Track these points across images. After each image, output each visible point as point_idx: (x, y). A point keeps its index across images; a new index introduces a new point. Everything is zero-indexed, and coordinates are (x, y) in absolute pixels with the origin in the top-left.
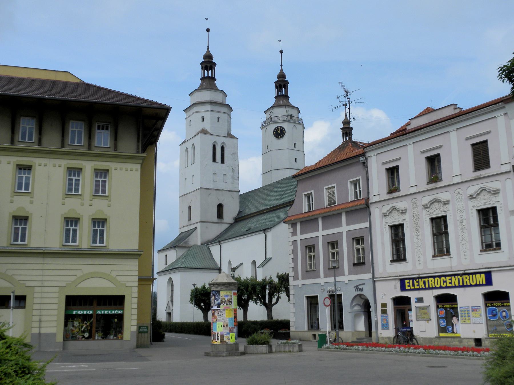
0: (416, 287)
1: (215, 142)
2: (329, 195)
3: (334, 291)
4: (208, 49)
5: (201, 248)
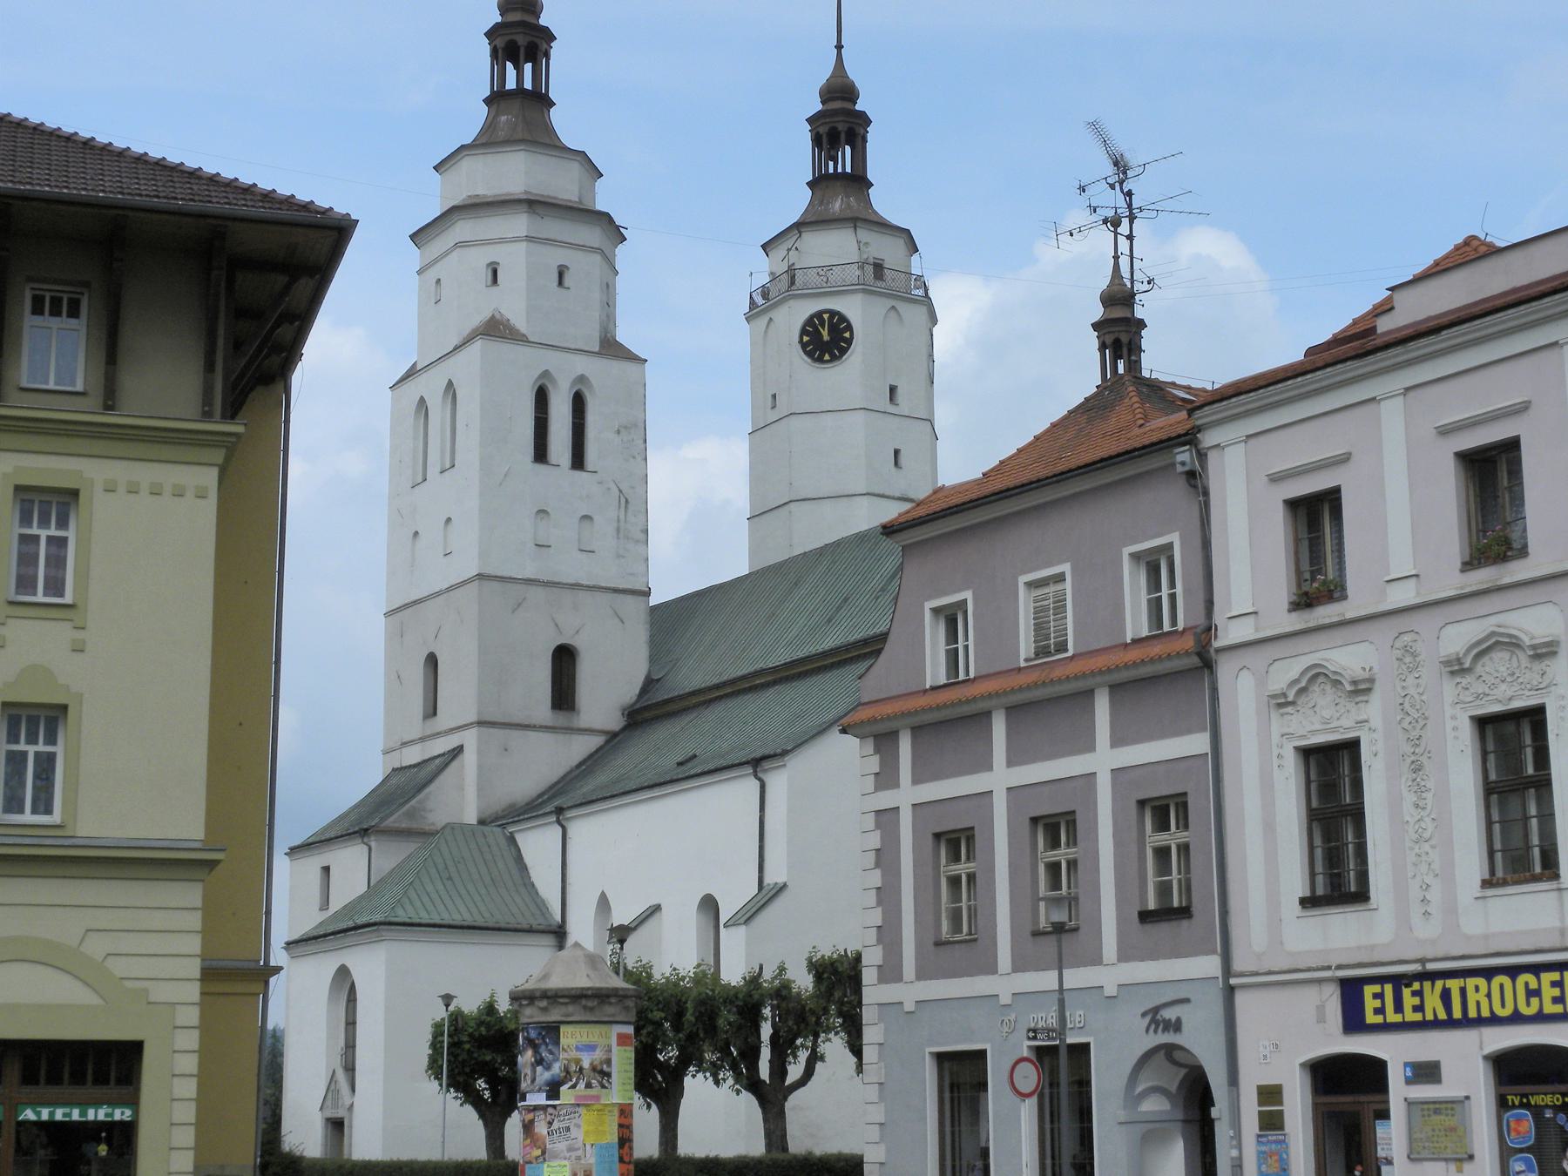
0: (1411, 1016)
1: (546, 374)
2: (1040, 612)
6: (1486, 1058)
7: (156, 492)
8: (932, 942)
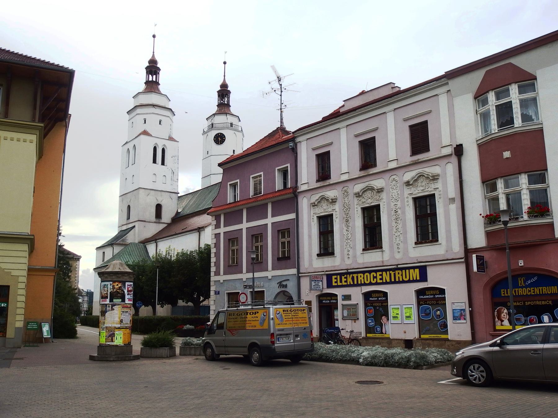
0: (344, 283)
1: (156, 144)
2: (255, 185)
3: (251, 286)
4: (153, 55)
5: (138, 247)
6: (362, 294)
7: (18, 140)
8: (227, 265)
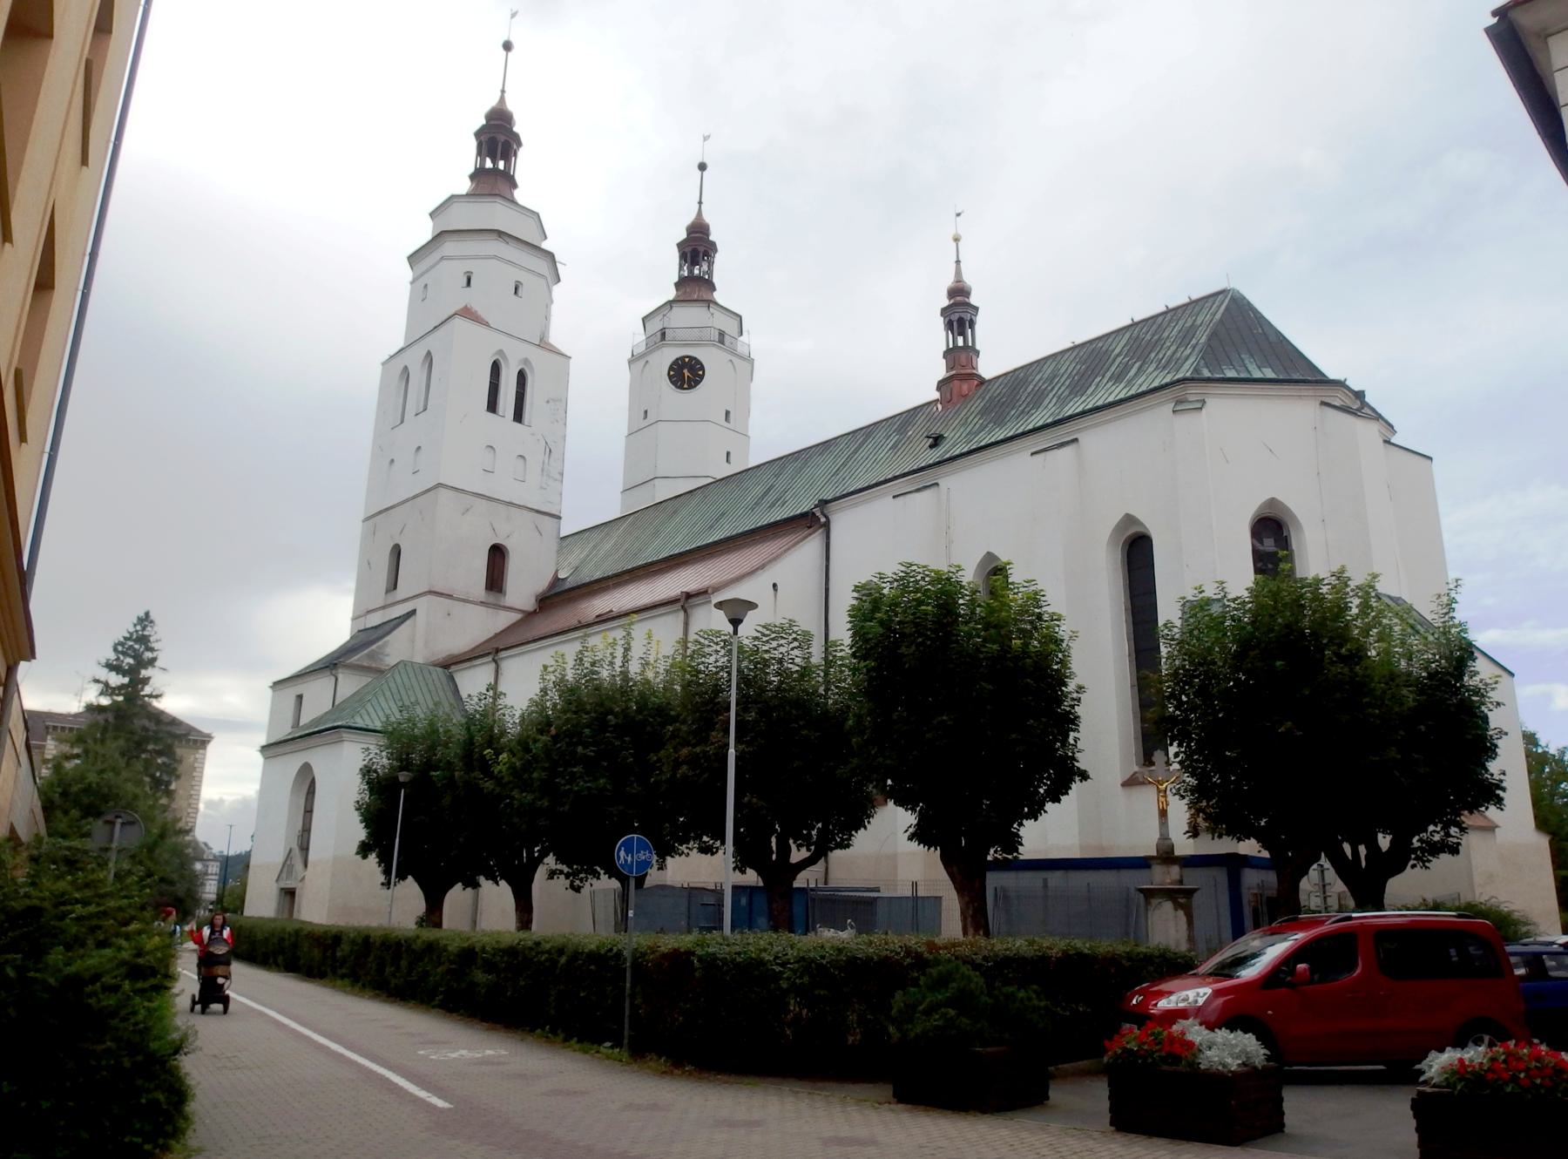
1: (501, 352)
